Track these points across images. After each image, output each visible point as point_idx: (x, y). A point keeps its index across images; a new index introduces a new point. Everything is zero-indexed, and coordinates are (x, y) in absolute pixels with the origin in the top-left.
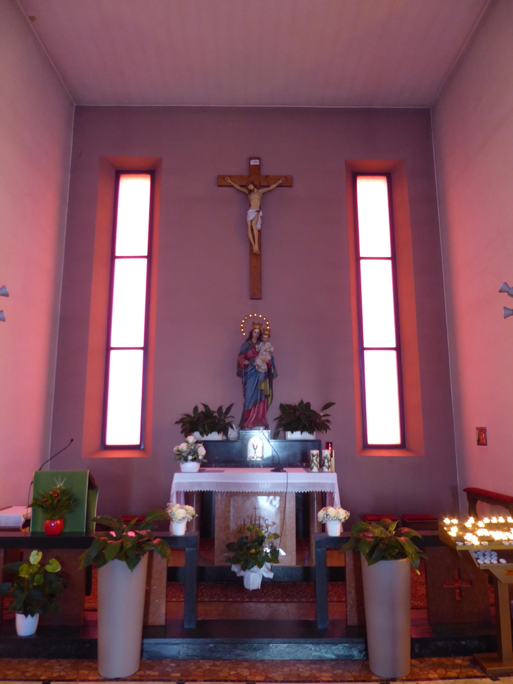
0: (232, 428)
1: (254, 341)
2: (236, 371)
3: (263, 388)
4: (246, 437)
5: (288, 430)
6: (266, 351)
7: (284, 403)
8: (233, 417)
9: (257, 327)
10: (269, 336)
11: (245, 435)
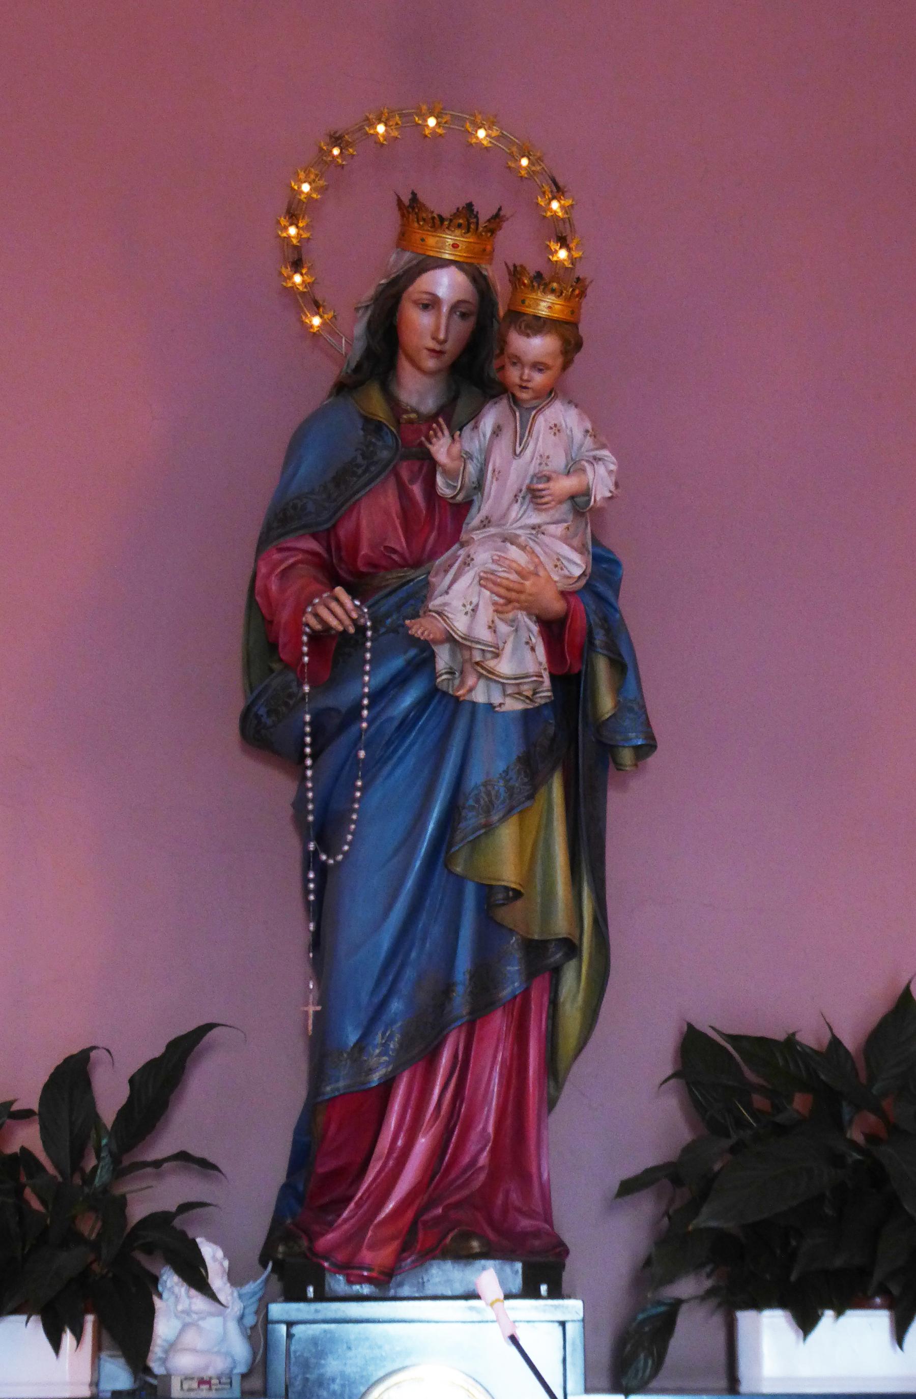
0: (195, 1276)
1: (417, 390)
2: (238, 704)
3: (508, 873)
4: (332, 1366)
5: (758, 1304)
6: (533, 495)
7: (717, 1018)
8: (206, 1166)
9: (449, 243)
10: (572, 345)
11: (320, 1349)
